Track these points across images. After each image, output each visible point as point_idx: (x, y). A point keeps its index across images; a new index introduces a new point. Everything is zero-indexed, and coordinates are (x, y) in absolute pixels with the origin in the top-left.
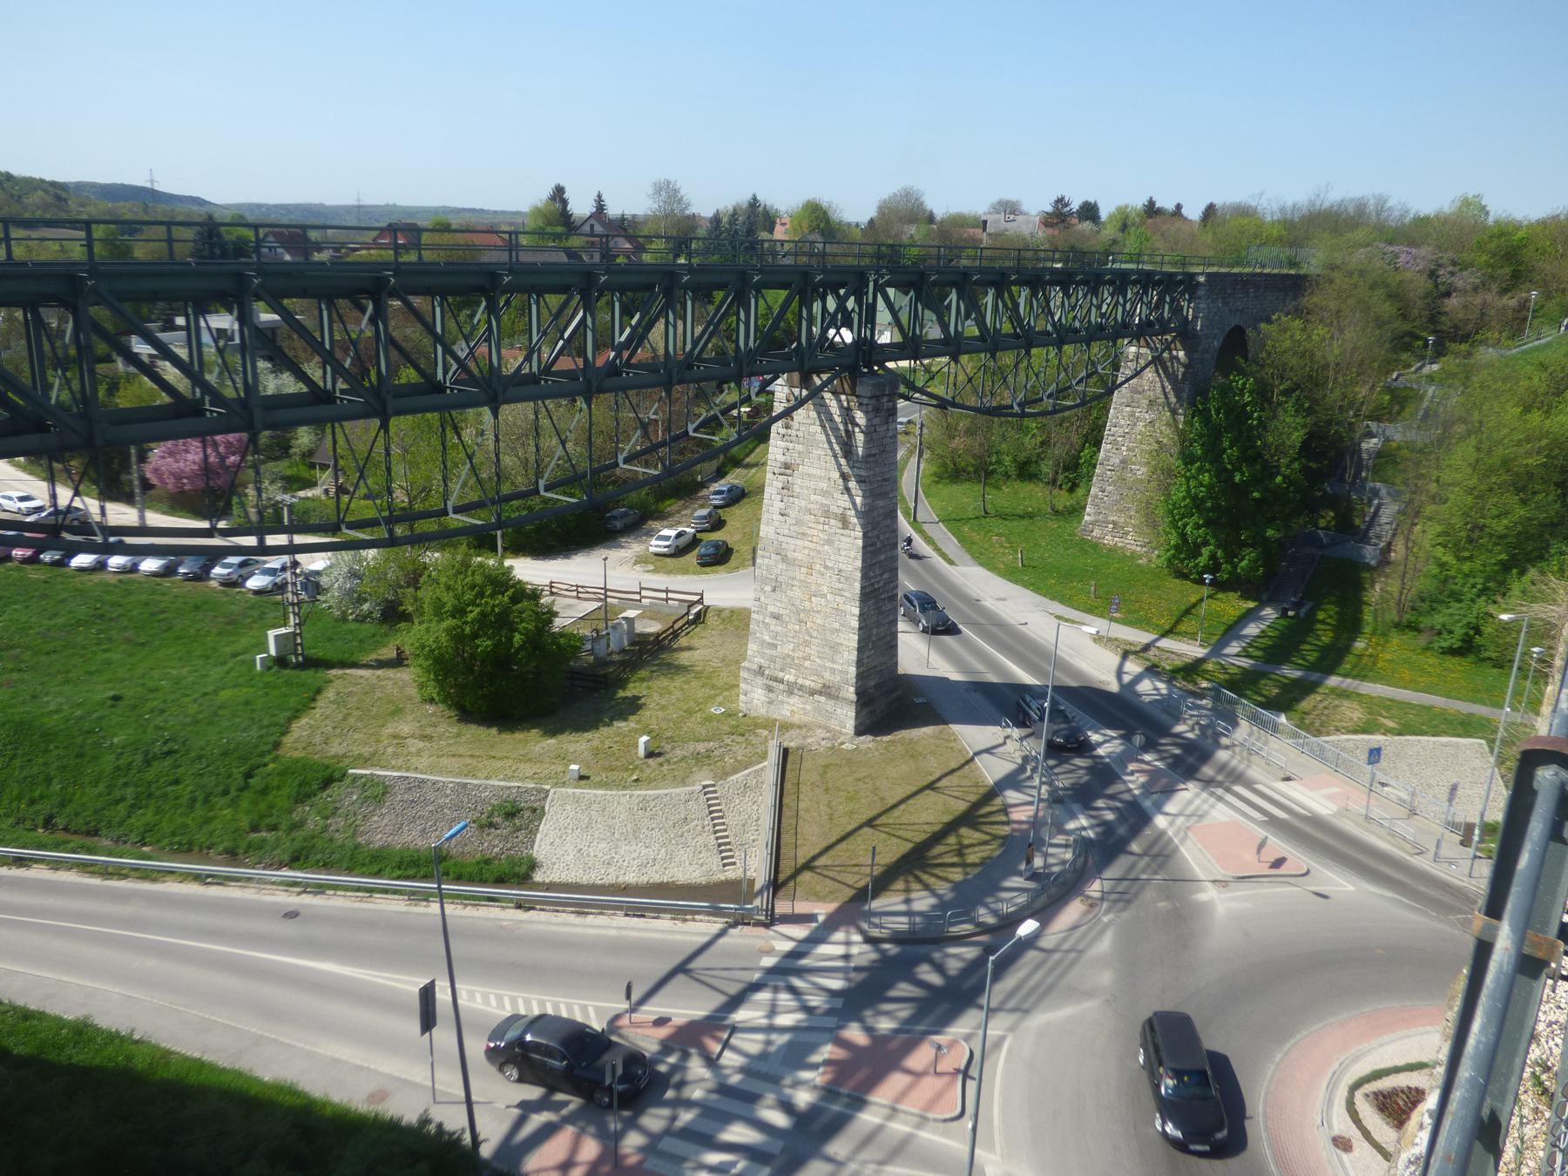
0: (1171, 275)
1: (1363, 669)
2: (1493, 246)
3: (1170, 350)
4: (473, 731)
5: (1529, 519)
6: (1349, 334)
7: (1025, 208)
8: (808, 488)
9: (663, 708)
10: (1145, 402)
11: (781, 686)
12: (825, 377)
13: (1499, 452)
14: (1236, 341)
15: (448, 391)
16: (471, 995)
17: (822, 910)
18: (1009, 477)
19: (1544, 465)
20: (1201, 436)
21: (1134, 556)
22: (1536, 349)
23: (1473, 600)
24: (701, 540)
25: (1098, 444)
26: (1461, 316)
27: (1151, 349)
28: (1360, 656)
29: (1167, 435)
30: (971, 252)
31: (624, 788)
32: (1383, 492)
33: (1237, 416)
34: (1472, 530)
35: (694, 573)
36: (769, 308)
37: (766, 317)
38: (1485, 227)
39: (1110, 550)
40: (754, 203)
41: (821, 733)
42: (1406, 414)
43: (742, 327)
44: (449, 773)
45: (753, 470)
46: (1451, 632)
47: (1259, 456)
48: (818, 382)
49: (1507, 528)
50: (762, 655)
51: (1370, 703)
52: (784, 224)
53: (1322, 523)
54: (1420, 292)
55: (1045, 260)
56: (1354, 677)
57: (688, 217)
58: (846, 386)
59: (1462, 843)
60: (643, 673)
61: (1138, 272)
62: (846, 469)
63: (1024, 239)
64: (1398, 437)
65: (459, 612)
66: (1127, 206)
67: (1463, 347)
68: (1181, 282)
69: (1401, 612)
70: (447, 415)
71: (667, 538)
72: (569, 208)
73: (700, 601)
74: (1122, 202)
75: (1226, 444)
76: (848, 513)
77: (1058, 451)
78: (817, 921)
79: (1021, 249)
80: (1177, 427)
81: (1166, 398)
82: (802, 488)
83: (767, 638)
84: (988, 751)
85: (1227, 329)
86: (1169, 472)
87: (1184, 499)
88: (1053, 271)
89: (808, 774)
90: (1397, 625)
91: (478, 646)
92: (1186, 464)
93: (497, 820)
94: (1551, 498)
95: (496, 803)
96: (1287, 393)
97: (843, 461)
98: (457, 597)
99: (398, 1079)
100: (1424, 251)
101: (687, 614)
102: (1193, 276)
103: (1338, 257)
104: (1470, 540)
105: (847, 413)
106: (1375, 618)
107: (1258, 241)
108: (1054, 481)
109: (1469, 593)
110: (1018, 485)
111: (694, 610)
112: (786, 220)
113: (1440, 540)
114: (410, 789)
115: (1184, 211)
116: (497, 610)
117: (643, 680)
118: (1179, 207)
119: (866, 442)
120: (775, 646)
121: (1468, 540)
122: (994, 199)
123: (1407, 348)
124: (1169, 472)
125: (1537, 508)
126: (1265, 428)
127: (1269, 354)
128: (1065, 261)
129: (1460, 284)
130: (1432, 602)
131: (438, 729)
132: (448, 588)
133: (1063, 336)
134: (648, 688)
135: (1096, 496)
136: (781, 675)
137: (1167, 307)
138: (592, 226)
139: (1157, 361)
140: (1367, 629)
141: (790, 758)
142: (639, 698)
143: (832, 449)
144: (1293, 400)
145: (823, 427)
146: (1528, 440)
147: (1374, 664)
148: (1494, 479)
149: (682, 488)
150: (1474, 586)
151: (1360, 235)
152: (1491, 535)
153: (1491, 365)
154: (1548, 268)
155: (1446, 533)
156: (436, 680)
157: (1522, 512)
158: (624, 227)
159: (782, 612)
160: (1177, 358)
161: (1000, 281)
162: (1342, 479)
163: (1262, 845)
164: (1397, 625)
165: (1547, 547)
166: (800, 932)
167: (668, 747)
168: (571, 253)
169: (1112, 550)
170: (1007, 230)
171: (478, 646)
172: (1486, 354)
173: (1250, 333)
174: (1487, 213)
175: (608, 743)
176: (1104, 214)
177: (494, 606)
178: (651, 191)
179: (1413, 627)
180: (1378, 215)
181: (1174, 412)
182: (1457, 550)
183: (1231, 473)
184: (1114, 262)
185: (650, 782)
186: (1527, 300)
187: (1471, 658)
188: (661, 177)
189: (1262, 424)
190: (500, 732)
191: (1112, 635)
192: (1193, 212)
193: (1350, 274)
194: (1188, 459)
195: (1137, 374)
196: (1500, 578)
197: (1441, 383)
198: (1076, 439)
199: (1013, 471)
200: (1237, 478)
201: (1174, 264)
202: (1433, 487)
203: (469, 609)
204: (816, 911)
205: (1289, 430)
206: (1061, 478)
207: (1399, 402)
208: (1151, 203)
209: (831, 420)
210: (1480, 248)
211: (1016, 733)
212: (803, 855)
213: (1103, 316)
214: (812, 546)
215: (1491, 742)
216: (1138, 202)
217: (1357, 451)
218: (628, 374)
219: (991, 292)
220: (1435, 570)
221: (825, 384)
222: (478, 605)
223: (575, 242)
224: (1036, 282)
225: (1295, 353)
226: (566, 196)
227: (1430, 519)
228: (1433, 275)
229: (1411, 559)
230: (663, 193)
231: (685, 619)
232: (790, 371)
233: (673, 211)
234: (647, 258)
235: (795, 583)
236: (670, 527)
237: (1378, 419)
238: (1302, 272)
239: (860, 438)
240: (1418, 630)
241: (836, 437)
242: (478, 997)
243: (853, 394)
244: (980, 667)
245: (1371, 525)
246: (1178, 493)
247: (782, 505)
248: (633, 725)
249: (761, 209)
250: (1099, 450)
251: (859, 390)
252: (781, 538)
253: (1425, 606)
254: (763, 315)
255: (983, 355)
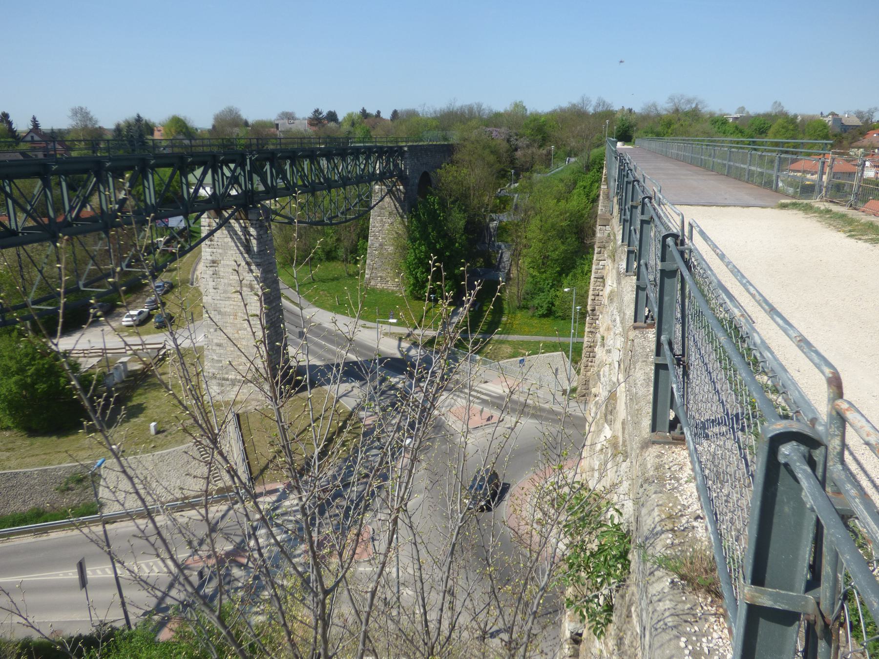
0: (391, 148)
1: (508, 330)
2: (531, 126)
3: (396, 186)
4: (39, 441)
5: (566, 250)
6: (477, 171)
7: (297, 115)
8: (228, 272)
9: (158, 407)
10: (387, 214)
11: (228, 382)
12: (230, 211)
13: (550, 221)
14: (426, 180)
15: (20, 235)
16: (94, 572)
17: (280, 486)
18: (321, 260)
19: (568, 225)
20: (417, 227)
21: (393, 292)
22: (557, 172)
23: (549, 291)
24: (153, 315)
25: (366, 238)
26: (523, 159)
27: (386, 186)
28: (505, 324)
29: (400, 228)
30: (275, 141)
31: (148, 452)
32: (503, 246)
33: (433, 215)
34: (544, 258)
35: (155, 333)
36: (161, 179)
37: (160, 185)
38: (527, 117)
39: (381, 291)
40: (139, 119)
41: (254, 403)
42: (508, 208)
43: (147, 190)
44: (34, 465)
45: (174, 273)
46: (542, 307)
47: (446, 234)
48: (226, 215)
49: (558, 255)
50: (214, 367)
51: (513, 344)
52: (159, 131)
53: (478, 264)
54: (504, 150)
55: (317, 143)
56: (505, 334)
57: (96, 129)
58: (242, 215)
59: (563, 395)
60: (140, 391)
61: (365, 147)
62: (249, 260)
63: (301, 133)
64: (505, 220)
65: (21, 370)
66: (353, 113)
67: (528, 174)
68: (396, 151)
69: (519, 301)
70: (22, 251)
71: (132, 316)
72: (13, 126)
73: (164, 347)
74: (350, 111)
75: (430, 230)
76: (253, 283)
77: (346, 243)
78: (279, 491)
79: (302, 138)
80: (405, 225)
81: (397, 210)
82: (224, 272)
83: (215, 358)
84: (345, 395)
85: (421, 174)
86: (404, 248)
87: (414, 260)
88: (320, 149)
89: (254, 422)
90: (519, 308)
91: (38, 389)
92: (412, 242)
93: (72, 485)
94: (574, 239)
95: (68, 476)
96: (453, 203)
97: (246, 256)
98: (17, 362)
99: (65, 622)
100: (503, 130)
101: (158, 355)
102: (401, 147)
103: (466, 135)
104: (543, 264)
105: (245, 230)
106: (509, 305)
107: (427, 129)
108: (346, 259)
109: (547, 288)
110: (327, 264)
111: (162, 353)
112: (161, 128)
113: (531, 265)
114: (9, 479)
115: (382, 115)
116: (46, 366)
117: (140, 395)
118: (379, 112)
119: (258, 244)
120: (221, 361)
121: (543, 263)
122: (280, 111)
123: (504, 176)
124: (404, 248)
125: (569, 245)
126: (447, 220)
127: (443, 184)
128: (325, 143)
129: (520, 144)
130: (532, 294)
131: (16, 444)
132: (11, 358)
133: (345, 182)
134: (146, 398)
135: (370, 264)
136: (226, 376)
137: (391, 164)
138: (32, 137)
139: (390, 192)
140: (506, 312)
141: (241, 418)
142: (142, 404)
143: (239, 249)
144: (457, 206)
145: (232, 238)
146: (561, 215)
147: (512, 327)
148: (549, 234)
149: (135, 287)
150: (548, 284)
151: (474, 123)
152: (552, 260)
153: (541, 181)
154: (556, 134)
155: (533, 262)
156: (11, 414)
157: (563, 248)
158: (54, 136)
159: (221, 342)
160: (399, 189)
161: (294, 157)
162: (484, 243)
163: (482, 411)
164: (519, 308)
165: (575, 262)
166: (274, 498)
167: (168, 427)
168: (23, 154)
169: (382, 290)
170: (291, 128)
171: (38, 389)
172: (536, 177)
173: (432, 174)
174: (526, 110)
175: (130, 432)
176: (340, 118)
177: (44, 364)
178: (70, 114)
179: (525, 307)
180: (479, 113)
181: (402, 217)
182: (539, 269)
183: (435, 244)
184: (351, 143)
185: (163, 446)
186: (550, 150)
187: (552, 317)
188: (76, 105)
189: (445, 219)
190: (59, 438)
191: (392, 331)
192: (386, 115)
193: (473, 143)
194: (413, 240)
195: (382, 199)
196: (558, 279)
197: (522, 192)
198: (354, 237)
199: (323, 257)
200: (438, 247)
201: (391, 142)
202: (524, 241)
203: (28, 368)
204: (278, 487)
205: (458, 220)
206: (349, 257)
207: (503, 203)
208: (364, 111)
209: (236, 234)
210: (526, 127)
211: (357, 384)
212: (263, 462)
213: (349, 172)
214: (234, 303)
215: (567, 353)
216: (357, 110)
217: (488, 228)
218: (160, 211)
219: (288, 162)
220: (531, 280)
221: (230, 217)
222: (33, 365)
223: (23, 146)
224: (312, 156)
225: (455, 183)
226: (10, 119)
227: (525, 256)
228: (508, 141)
229: (520, 275)
230: (78, 115)
231: (157, 359)
232: (208, 210)
233: (86, 126)
234: (74, 154)
235: (228, 325)
236: (134, 309)
237: (495, 212)
238: (450, 143)
239: (254, 242)
240: (528, 309)
241: (240, 243)
242: (99, 572)
243: (247, 219)
244: (330, 357)
245: (500, 262)
246: (411, 257)
247: (214, 284)
248: (143, 419)
249: (144, 122)
250: (367, 241)
251: (250, 217)
252: (216, 302)
253: (529, 297)
254: (158, 184)
255: (324, 192)
